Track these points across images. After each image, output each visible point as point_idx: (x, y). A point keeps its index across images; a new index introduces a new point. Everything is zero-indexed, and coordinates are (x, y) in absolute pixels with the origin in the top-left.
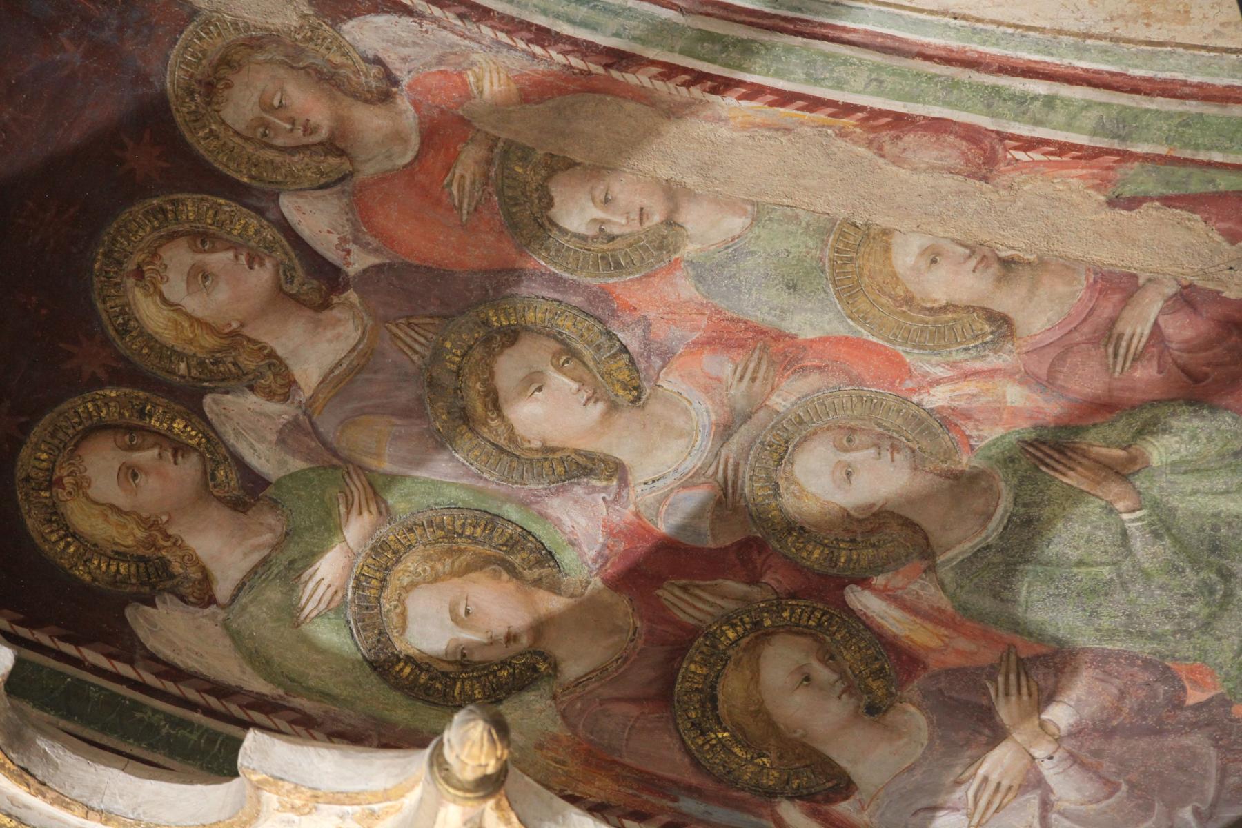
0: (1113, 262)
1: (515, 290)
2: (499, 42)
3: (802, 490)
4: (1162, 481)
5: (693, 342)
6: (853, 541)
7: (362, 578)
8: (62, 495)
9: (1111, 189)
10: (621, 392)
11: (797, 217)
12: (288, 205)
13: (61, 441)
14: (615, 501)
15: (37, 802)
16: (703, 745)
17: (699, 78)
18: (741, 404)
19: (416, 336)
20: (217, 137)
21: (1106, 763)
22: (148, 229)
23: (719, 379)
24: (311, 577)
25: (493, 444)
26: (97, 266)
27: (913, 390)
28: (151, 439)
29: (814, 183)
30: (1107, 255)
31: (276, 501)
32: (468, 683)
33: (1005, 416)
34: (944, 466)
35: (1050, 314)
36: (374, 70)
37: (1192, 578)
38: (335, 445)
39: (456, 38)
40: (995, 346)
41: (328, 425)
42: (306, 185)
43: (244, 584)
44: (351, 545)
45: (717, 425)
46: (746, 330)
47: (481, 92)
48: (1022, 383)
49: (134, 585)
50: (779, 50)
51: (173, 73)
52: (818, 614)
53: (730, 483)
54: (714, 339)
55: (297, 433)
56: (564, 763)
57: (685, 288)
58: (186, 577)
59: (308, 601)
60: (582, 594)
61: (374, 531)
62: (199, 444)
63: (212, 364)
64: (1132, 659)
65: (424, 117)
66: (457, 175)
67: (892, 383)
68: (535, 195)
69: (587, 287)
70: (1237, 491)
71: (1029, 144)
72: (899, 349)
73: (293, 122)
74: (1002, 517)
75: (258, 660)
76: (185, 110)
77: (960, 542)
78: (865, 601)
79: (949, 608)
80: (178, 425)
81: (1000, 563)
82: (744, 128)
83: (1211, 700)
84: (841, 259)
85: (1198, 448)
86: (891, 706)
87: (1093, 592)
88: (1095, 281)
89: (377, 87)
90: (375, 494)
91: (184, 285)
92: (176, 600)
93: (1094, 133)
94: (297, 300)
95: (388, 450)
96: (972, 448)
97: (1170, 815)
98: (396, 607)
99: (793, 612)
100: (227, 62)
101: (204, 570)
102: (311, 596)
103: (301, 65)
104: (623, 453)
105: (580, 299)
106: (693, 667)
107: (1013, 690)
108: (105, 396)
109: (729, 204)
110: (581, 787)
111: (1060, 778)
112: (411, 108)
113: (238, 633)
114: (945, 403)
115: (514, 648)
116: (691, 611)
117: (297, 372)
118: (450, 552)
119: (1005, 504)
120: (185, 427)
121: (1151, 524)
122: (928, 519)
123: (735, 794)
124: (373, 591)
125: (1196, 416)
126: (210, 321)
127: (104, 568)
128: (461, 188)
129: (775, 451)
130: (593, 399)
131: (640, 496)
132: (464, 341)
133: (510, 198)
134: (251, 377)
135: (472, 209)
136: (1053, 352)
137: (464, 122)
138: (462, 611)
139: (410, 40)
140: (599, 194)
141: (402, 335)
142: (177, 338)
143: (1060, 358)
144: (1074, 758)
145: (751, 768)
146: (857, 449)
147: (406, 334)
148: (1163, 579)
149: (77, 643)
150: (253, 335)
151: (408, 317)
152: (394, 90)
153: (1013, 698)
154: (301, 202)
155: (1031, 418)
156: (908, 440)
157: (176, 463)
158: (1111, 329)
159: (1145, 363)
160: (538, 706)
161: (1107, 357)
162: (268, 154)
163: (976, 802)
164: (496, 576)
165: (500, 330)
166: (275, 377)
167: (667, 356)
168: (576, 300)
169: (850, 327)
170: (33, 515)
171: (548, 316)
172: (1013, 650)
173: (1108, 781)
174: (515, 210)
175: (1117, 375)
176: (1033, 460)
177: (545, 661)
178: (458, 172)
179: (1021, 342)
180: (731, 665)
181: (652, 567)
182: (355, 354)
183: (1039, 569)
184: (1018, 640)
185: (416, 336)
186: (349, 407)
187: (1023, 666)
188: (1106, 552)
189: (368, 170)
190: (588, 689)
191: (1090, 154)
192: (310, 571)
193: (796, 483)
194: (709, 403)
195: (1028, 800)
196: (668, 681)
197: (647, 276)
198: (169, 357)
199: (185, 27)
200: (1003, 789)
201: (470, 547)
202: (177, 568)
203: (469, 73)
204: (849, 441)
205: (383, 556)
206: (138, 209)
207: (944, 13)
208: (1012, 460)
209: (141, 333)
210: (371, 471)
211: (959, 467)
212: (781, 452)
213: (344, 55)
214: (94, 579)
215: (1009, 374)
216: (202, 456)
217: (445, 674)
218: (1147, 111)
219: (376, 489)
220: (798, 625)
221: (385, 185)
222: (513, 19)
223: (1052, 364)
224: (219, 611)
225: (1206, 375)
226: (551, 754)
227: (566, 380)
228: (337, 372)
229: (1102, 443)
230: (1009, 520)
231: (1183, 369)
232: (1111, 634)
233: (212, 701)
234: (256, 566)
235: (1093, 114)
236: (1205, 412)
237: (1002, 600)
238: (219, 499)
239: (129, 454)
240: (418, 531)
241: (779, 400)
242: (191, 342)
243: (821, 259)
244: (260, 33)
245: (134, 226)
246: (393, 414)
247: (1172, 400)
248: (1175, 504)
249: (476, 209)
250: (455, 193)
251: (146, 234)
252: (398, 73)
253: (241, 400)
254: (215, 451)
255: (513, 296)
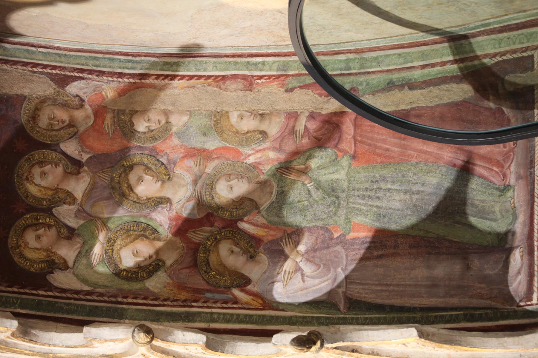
1: (129, 153)
2: (109, 80)
3: (220, 196)
4: (316, 173)
8: (22, 249)
9: (285, 87)
11: (202, 113)
14: (170, 210)
15: (36, 346)
17: (166, 76)
18: (198, 173)
20: (39, 132)
21: (316, 259)
23: (190, 167)
27: (244, 159)
28: (41, 226)
29: (204, 101)
30: (288, 107)
34: (257, 180)
36: (77, 99)
37: (329, 200)
39: (97, 83)
40: (263, 141)
41: (87, 208)
42: (66, 139)
48: (273, 151)
50: (186, 63)
56: (172, 290)
57: (175, 141)
58: (60, 263)
64: (317, 227)
71: (261, 77)
72: (237, 147)
73: (58, 121)
75: (84, 281)
77: (265, 202)
78: (244, 226)
79: (266, 223)
80: (47, 220)
82: (182, 89)
83: (340, 235)
87: (304, 209)
90: (105, 224)
93: (277, 71)
94: (71, 173)
95: (105, 211)
96: (263, 173)
97: (335, 271)
100: (37, 109)
101: (64, 260)
104: (169, 196)
107: (288, 243)
109: (182, 113)
110: (178, 296)
114: (253, 161)
115: (152, 260)
116: (197, 238)
117: (76, 195)
118: (128, 236)
119: (275, 188)
122: (255, 197)
128: (108, 127)
130: (157, 181)
131: (176, 207)
136: (279, 140)
137: (104, 107)
138: (135, 252)
140: (146, 119)
143: (282, 141)
144: (308, 260)
145: (223, 281)
146: (232, 180)
148: (321, 202)
149: (36, 290)
153: (288, 246)
154: (65, 144)
160: (162, 275)
163: (284, 278)
164: (142, 240)
165: (128, 167)
166: (70, 198)
167: (175, 163)
168: (147, 152)
178: (106, 123)
180: (211, 252)
181: (184, 227)
184: (286, 228)
186: (92, 201)
189: (82, 129)
191: (278, 77)
193: (218, 194)
196: (195, 260)
197: (165, 140)
198: (41, 201)
200: (290, 273)
202: (57, 261)
205: (111, 242)
206: (23, 160)
207: (229, 47)
209: (32, 196)
212: (212, 186)
215: (269, 149)
216: (56, 227)
217: (135, 272)
218: (290, 61)
219: (104, 223)
221: (87, 132)
222: (111, 72)
223: (280, 143)
225: (322, 138)
227: (149, 177)
229: (297, 164)
231: (315, 138)
232: (311, 221)
233: (75, 296)
235: (276, 64)
242: (45, 194)
245: (22, 166)
251: (26, 167)
254: (59, 224)
255: (129, 155)
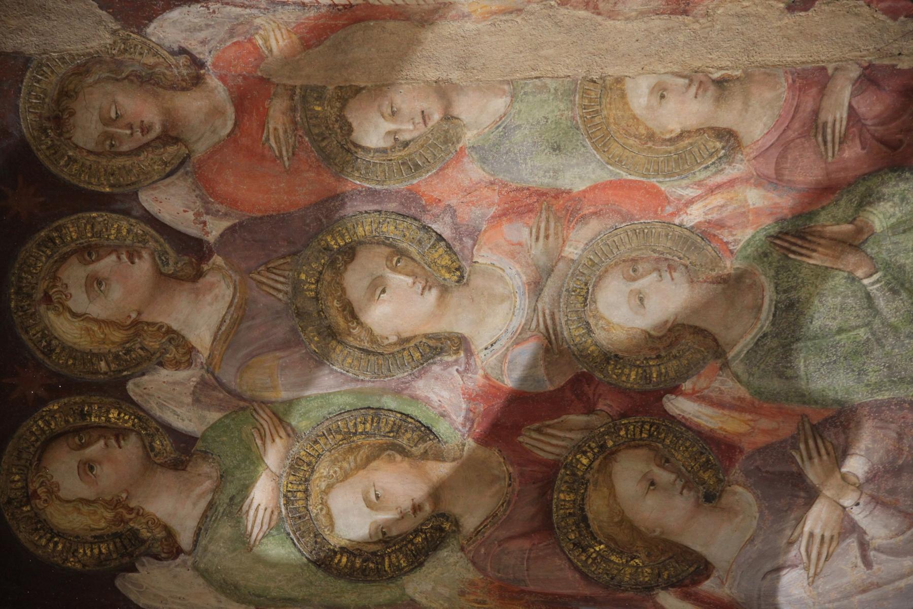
0: (803, 59)
1: (342, 213)
3: (609, 323)
4: (887, 244)
5: (492, 217)
6: (659, 357)
7: (289, 494)
8: (40, 504)
10: (447, 276)
12: (148, 200)
13: (27, 460)
14: (466, 370)
16: (587, 560)
18: (543, 261)
19: (277, 278)
20: (76, 161)
22: (44, 259)
23: (520, 244)
24: (250, 506)
25: (360, 349)
26: (13, 305)
27: (673, 214)
29: (551, 51)
30: (796, 55)
31: (206, 452)
32: (393, 556)
33: (751, 218)
34: (714, 273)
35: (765, 119)
36: (182, 60)
38: (239, 390)
39: (239, 9)
40: (728, 158)
41: (228, 376)
42: (156, 178)
43: (200, 529)
44: (274, 470)
45: (529, 284)
46: (530, 195)
47: (271, 51)
48: (758, 185)
49: (116, 559)
51: (25, 119)
52: (647, 427)
53: (551, 331)
54: (507, 209)
55: (208, 389)
57: (473, 171)
59: (253, 527)
60: (461, 456)
61: (288, 452)
62: (133, 425)
63: (125, 354)
65: (232, 87)
66: (271, 130)
67: (656, 212)
68: (337, 126)
69: (397, 192)
70: (909, 383)
73: (130, 126)
74: (770, 306)
76: (43, 147)
78: (681, 406)
79: (748, 396)
80: (113, 414)
81: (777, 347)
82: (485, 19)
84: (588, 113)
85: (909, 208)
86: (722, 491)
87: (856, 353)
88: (794, 81)
89: (188, 74)
91: (85, 296)
92: (151, 560)
96: (732, 252)
98: (321, 510)
99: (627, 430)
101: (166, 528)
102: (254, 521)
103: (124, 75)
104: (462, 328)
105: (394, 205)
106: (562, 496)
107: (814, 454)
108: (50, 411)
109: (488, 88)
111: (869, 519)
112: (220, 83)
113: (206, 570)
114: (701, 219)
115: (421, 516)
116: (548, 448)
117: (193, 339)
118: (351, 450)
119: (769, 295)
120: (119, 415)
121: (887, 284)
122: (711, 322)
123: (621, 595)
124: (301, 502)
125: (901, 180)
126: (113, 319)
127: (89, 553)
129: (579, 294)
130: (427, 287)
132: (313, 269)
133: (317, 135)
134: (158, 355)
135: (290, 154)
136: (775, 153)
137: (264, 81)
138: (373, 497)
139: (203, 24)
140: (387, 110)
141: (265, 280)
142: (92, 343)
143: (782, 156)
144: (876, 500)
145: (628, 570)
146: (642, 276)
147: (268, 278)
150: (150, 320)
151: (266, 263)
152: (202, 72)
153: (816, 460)
154: (155, 193)
155: (771, 214)
156: (680, 258)
157: (120, 447)
158: (816, 120)
159: (850, 143)
160: (452, 560)
161: (819, 146)
162: (120, 161)
164: (391, 460)
165: (339, 251)
166: (175, 348)
167: (474, 234)
168: (392, 206)
169: (611, 171)
170: (22, 529)
171: (375, 226)
172: (806, 419)
173: (908, 514)
174: (324, 144)
175: (830, 159)
176: (782, 251)
177: (447, 520)
178: (271, 127)
179: (747, 150)
180: (591, 487)
181: (510, 418)
182: (233, 308)
183: (809, 344)
185: (277, 278)
186: (241, 354)
187: (817, 431)
188: (858, 316)
189: (201, 148)
190: (486, 535)
192: (248, 501)
193: (602, 318)
194: (517, 266)
195: (848, 545)
196: (546, 511)
197: (441, 169)
198: (90, 361)
199: (24, 75)
200: (827, 540)
201: (365, 442)
202: (145, 534)
203: (257, 37)
204: (635, 271)
205: (300, 469)
206: (31, 245)
208: (766, 255)
209: (63, 349)
210: (272, 403)
211: (726, 272)
213: (154, 55)
214: (84, 565)
215: (745, 180)
216: (139, 433)
217: (374, 554)
219: (280, 416)
220: (634, 440)
223: (777, 163)
224: (187, 557)
225: (901, 141)
226: (472, 597)
227: (402, 277)
228: (223, 328)
229: (832, 222)
230: (776, 307)
231: (881, 141)
232: (879, 387)
234: (205, 511)
236: (908, 175)
237: (787, 378)
238: (161, 465)
239: (82, 452)
240: (322, 441)
241: (571, 250)
243: (573, 118)
244: (83, 59)
245: (32, 260)
246: (276, 350)
247: (880, 170)
248: (902, 261)
249: (294, 154)
250: (274, 145)
252: (201, 56)
253: (156, 377)
254: (149, 427)
255: (342, 218)
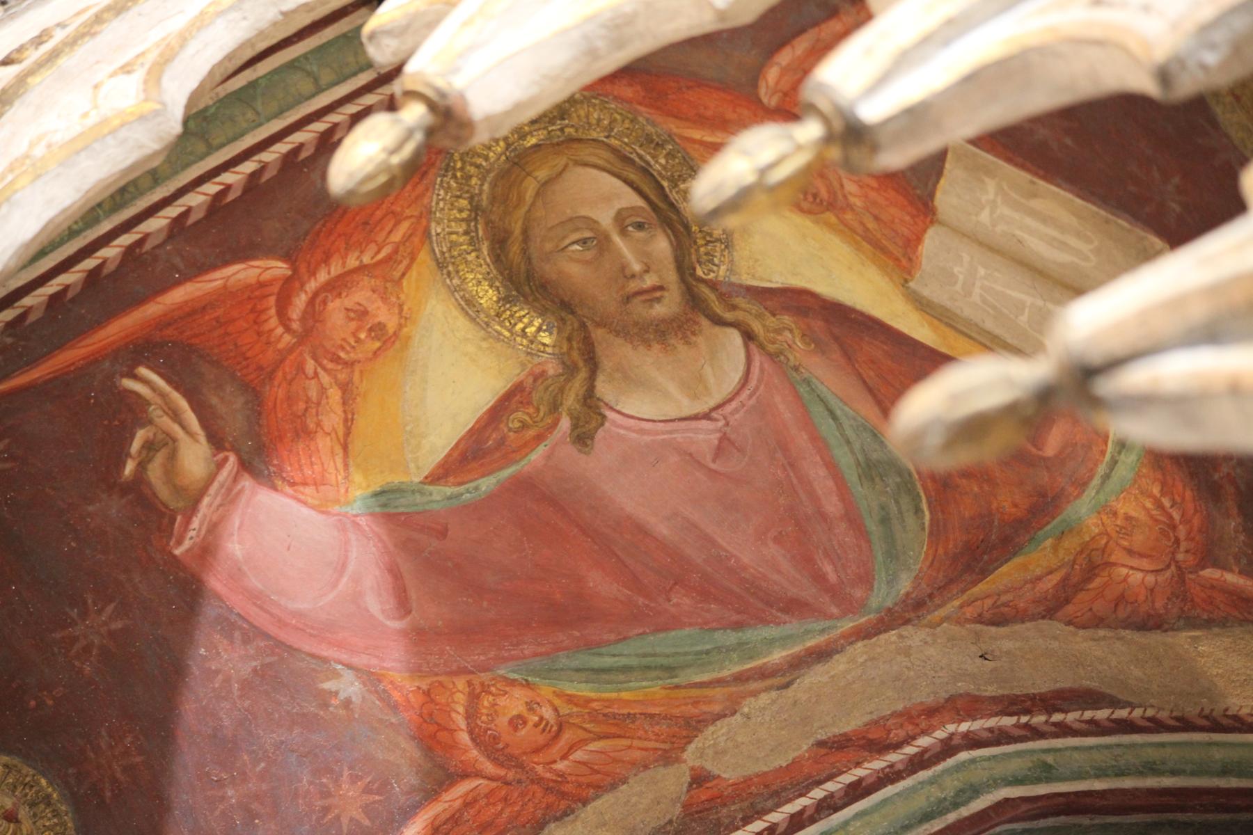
26: (43, 782)
227: (1004, 569)
255: (983, 182)
